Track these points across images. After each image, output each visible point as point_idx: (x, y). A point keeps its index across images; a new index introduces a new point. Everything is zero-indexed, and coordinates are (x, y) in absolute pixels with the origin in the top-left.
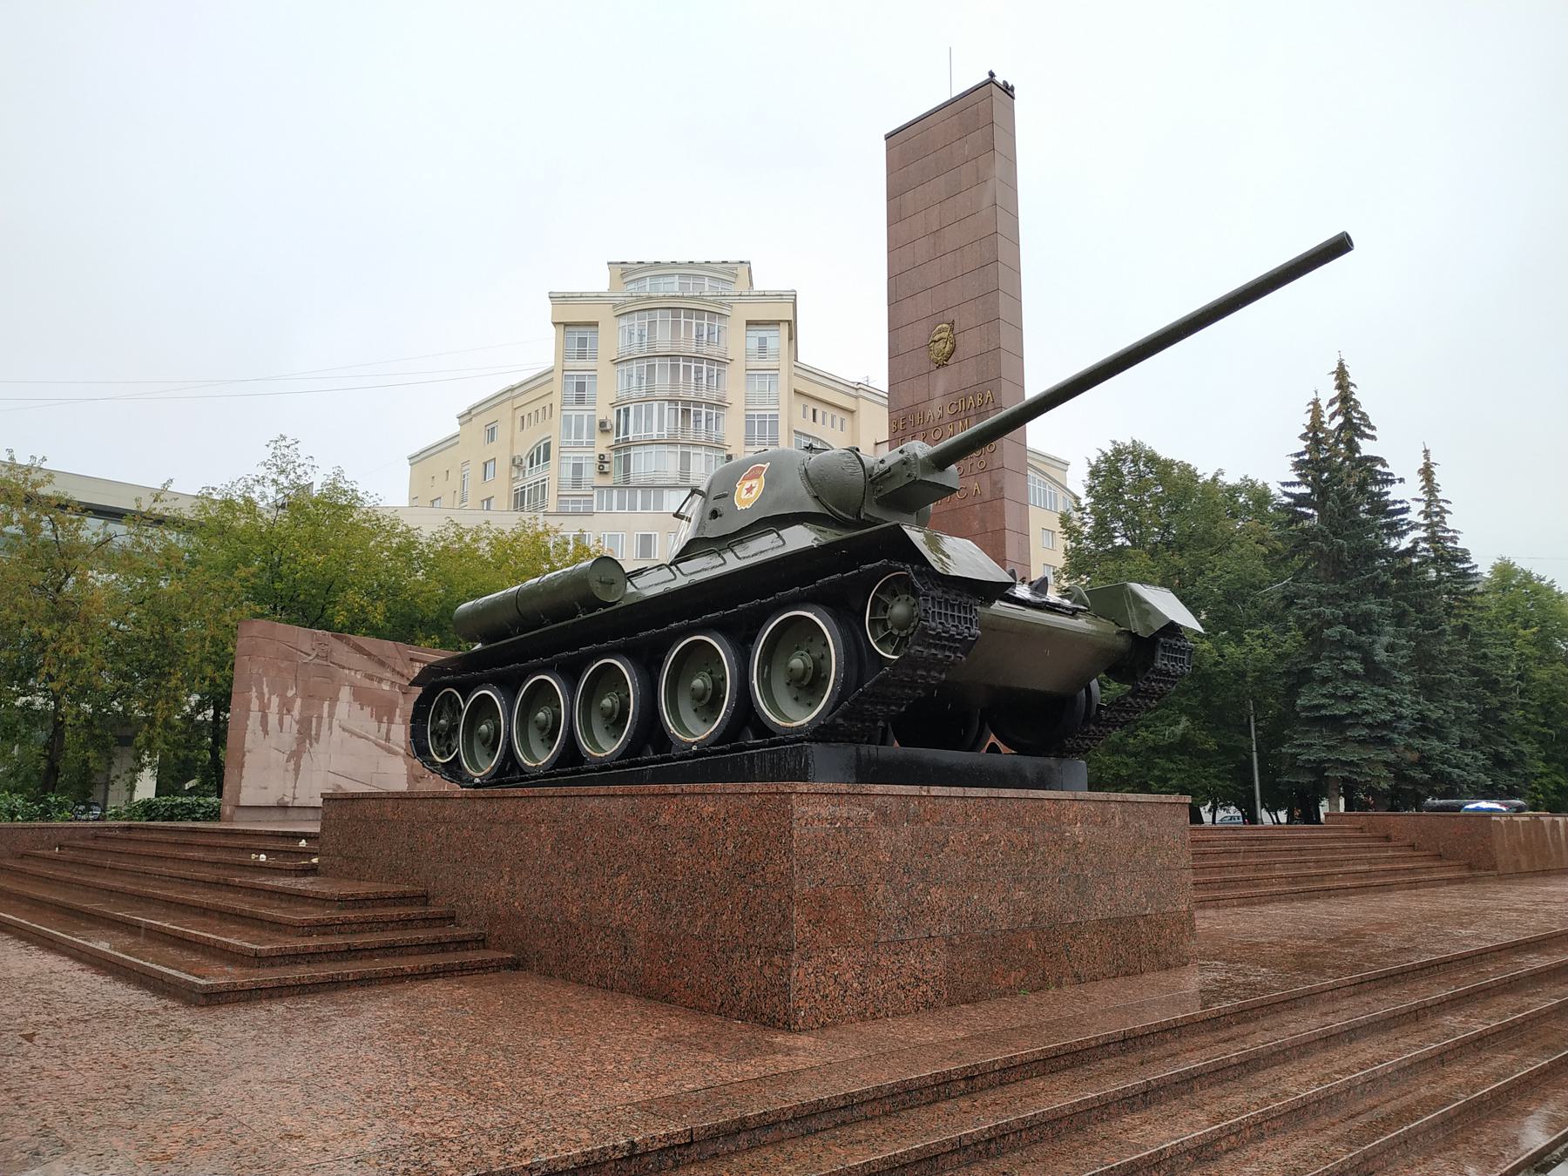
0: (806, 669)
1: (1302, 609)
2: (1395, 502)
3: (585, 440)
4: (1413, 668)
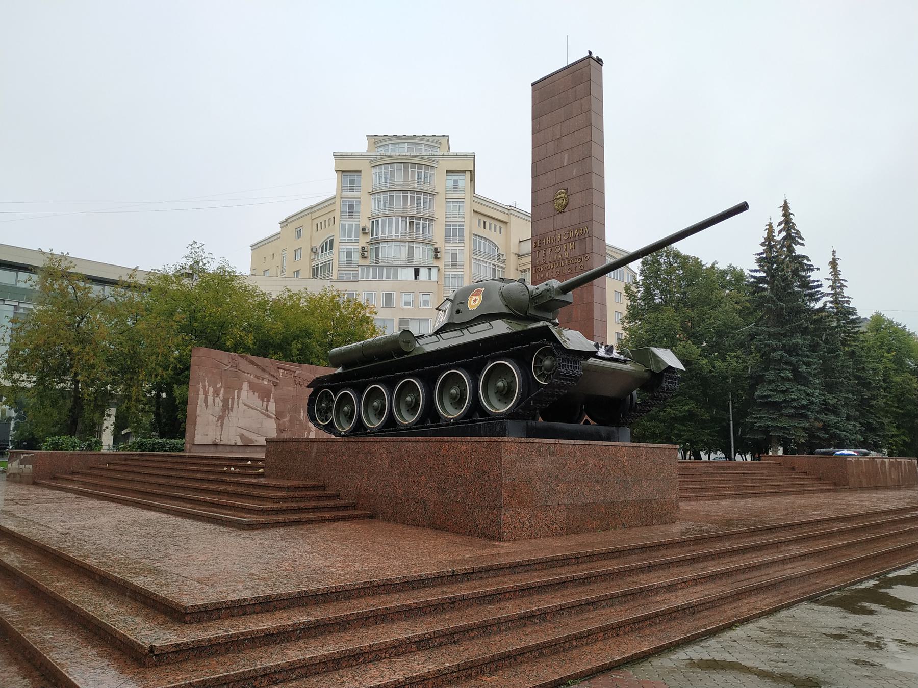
0: (504, 387)
2: (814, 281)
3: (353, 238)
4: (821, 375)
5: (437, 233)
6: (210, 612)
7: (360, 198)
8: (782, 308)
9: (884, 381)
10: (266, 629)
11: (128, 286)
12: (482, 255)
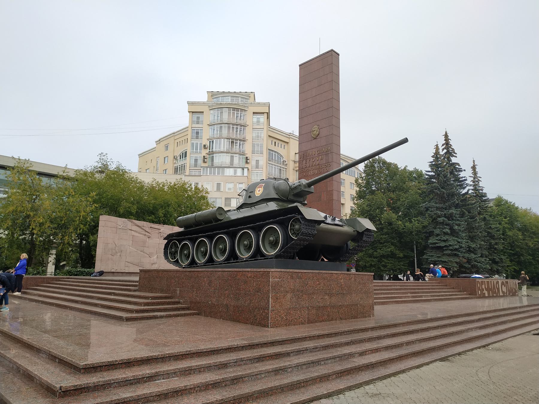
0: (274, 240)
1: (431, 212)
2: (462, 177)
3: (199, 151)
5: (248, 148)
6: (96, 368)
7: (203, 128)
8: (444, 193)
9: (503, 234)
10: (127, 377)
11: (64, 178)
12: (274, 161)
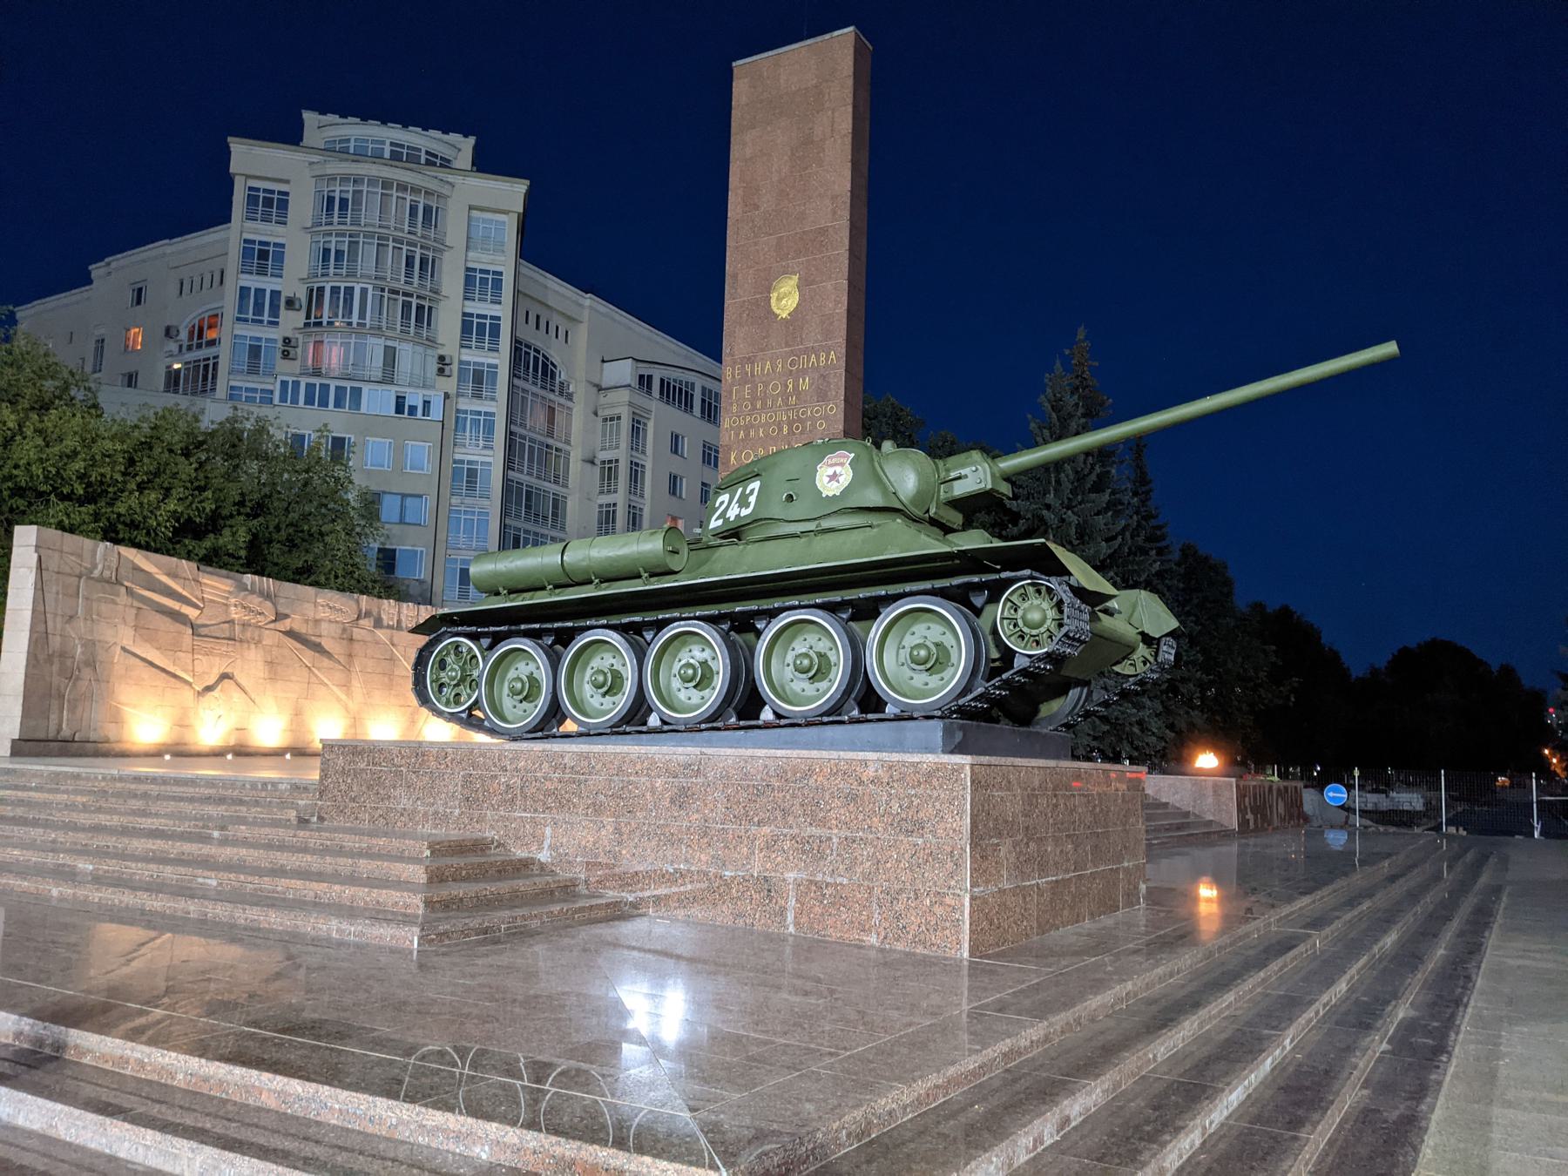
7: (287, 182)
